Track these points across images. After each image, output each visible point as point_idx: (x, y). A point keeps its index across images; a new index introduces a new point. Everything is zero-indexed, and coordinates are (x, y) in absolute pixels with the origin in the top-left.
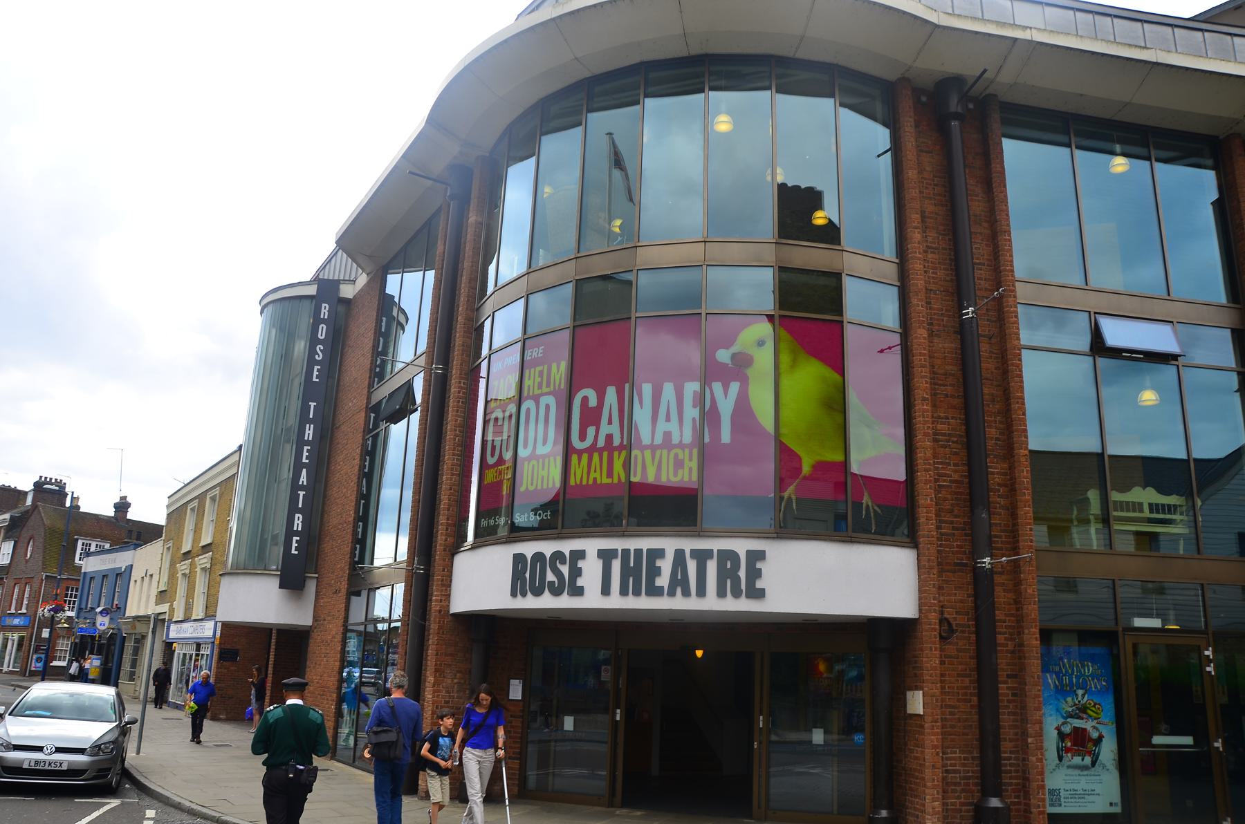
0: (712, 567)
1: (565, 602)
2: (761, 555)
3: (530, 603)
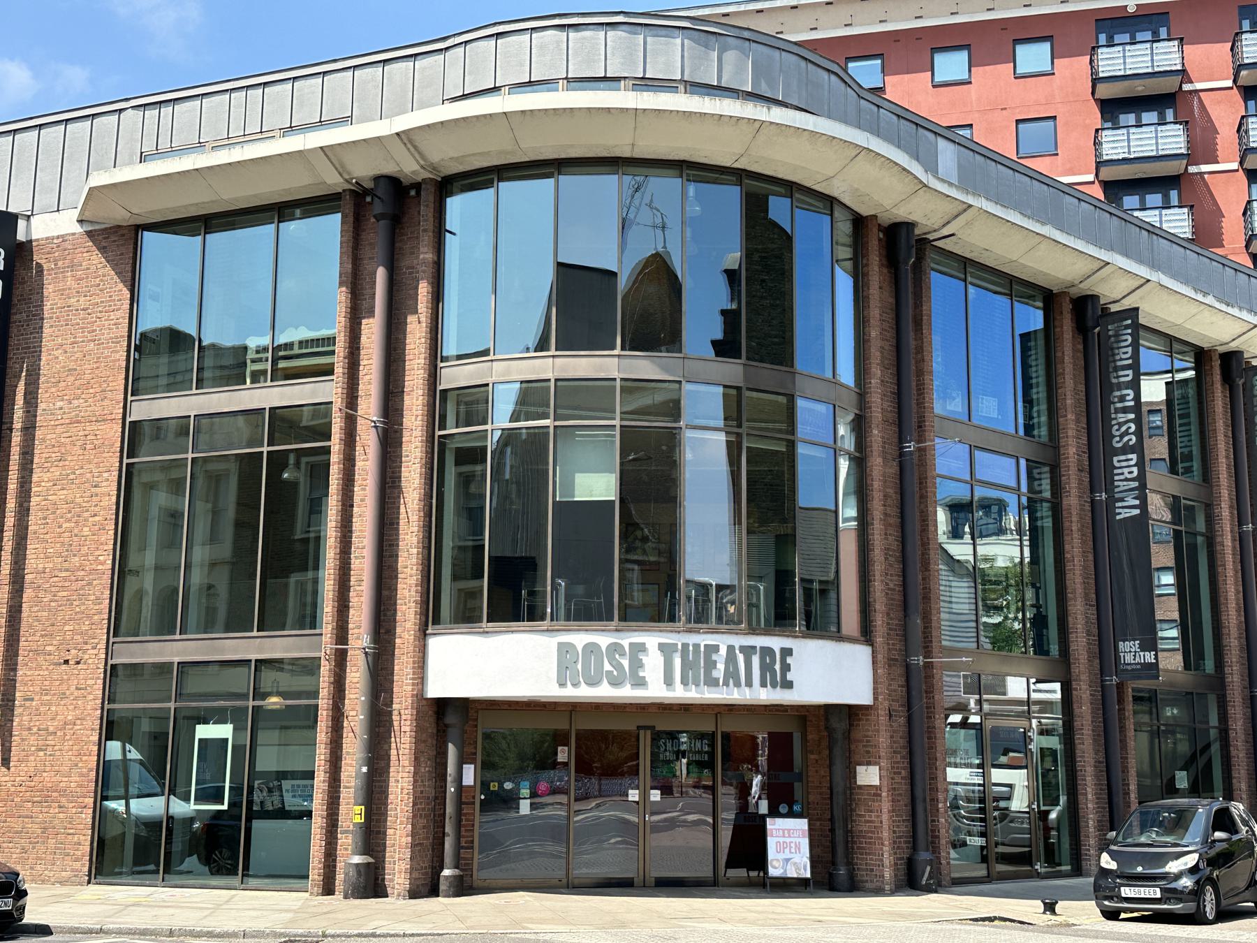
0: (756, 660)
1: (626, 693)
2: (787, 652)
3: (584, 692)
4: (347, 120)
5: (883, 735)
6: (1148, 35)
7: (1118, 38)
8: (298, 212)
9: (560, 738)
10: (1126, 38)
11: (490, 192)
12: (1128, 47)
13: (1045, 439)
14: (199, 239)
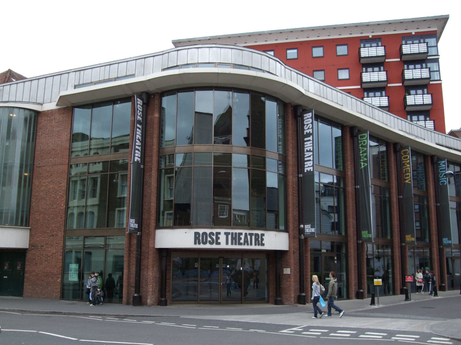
0: (253, 237)
1: (214, 246)
2: (263, 235)
3: (202, 246)
4: (133, 76)
5: (293, 259)
6: (417, 41)
7: (408, 42)
8: (119, 102)
9: (196, 260)
10: (411, 42)
11: (175, 96)
12: (411, 45)
13: (342, 170)
14: (90, 110)
